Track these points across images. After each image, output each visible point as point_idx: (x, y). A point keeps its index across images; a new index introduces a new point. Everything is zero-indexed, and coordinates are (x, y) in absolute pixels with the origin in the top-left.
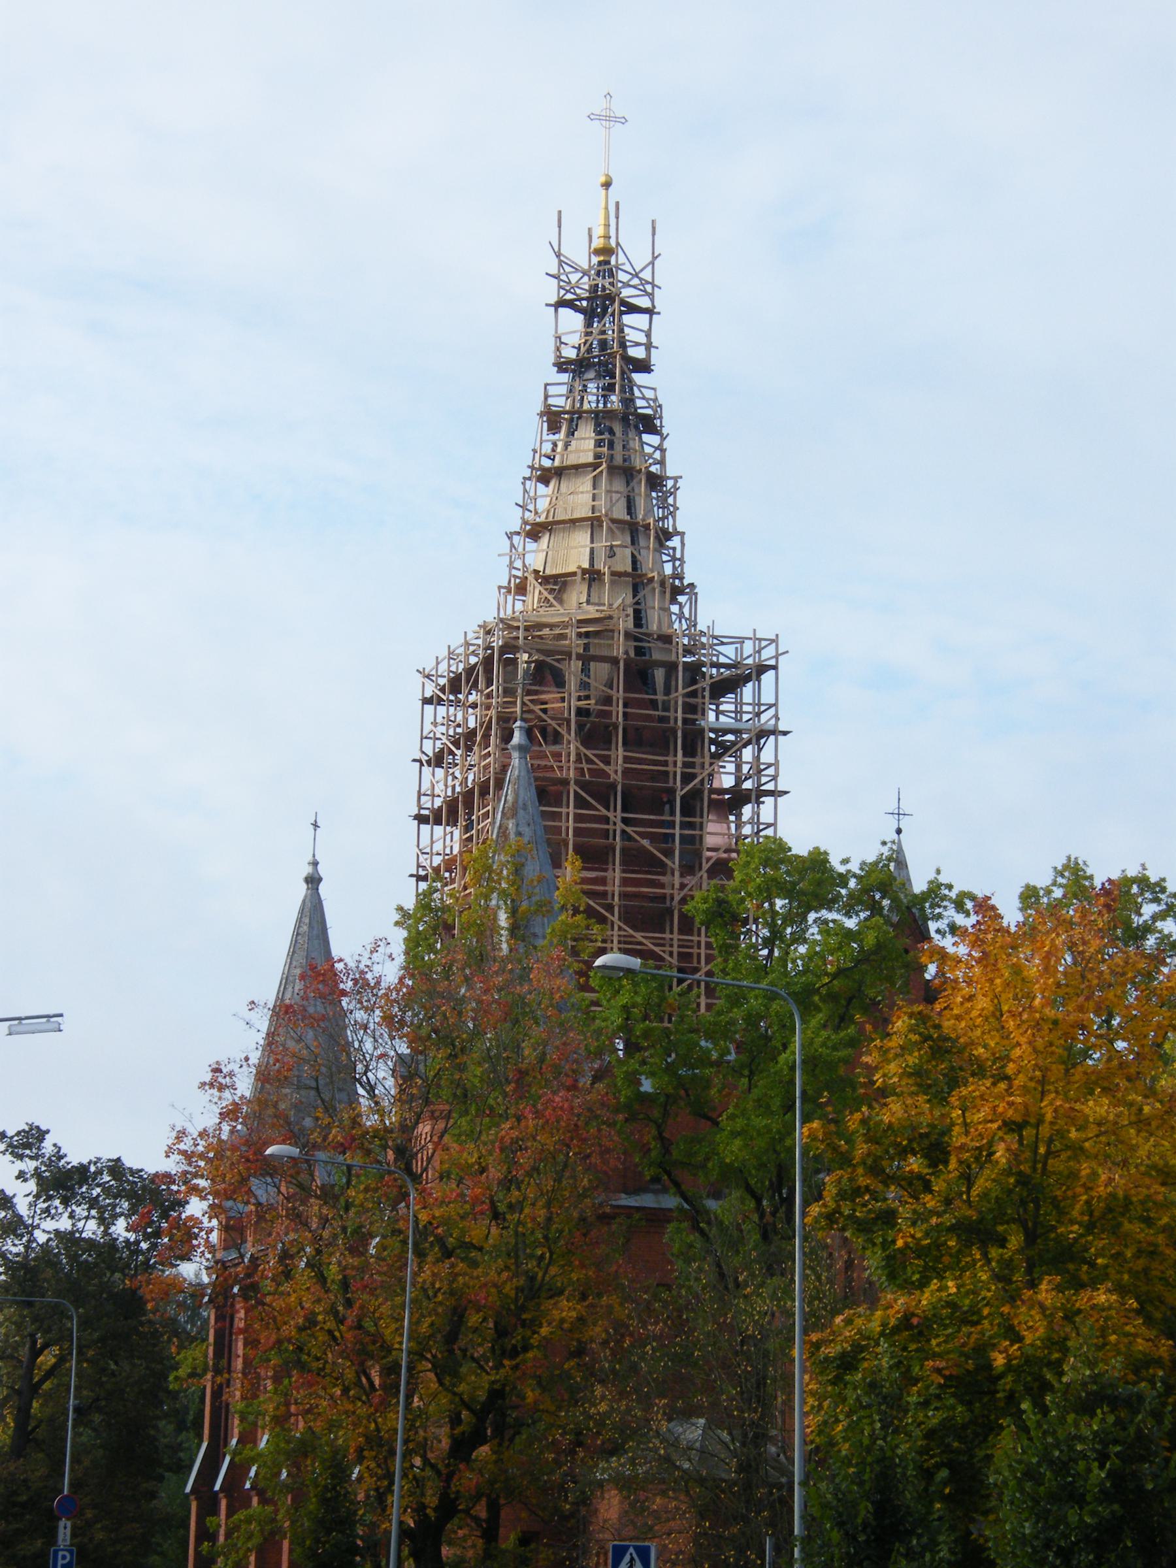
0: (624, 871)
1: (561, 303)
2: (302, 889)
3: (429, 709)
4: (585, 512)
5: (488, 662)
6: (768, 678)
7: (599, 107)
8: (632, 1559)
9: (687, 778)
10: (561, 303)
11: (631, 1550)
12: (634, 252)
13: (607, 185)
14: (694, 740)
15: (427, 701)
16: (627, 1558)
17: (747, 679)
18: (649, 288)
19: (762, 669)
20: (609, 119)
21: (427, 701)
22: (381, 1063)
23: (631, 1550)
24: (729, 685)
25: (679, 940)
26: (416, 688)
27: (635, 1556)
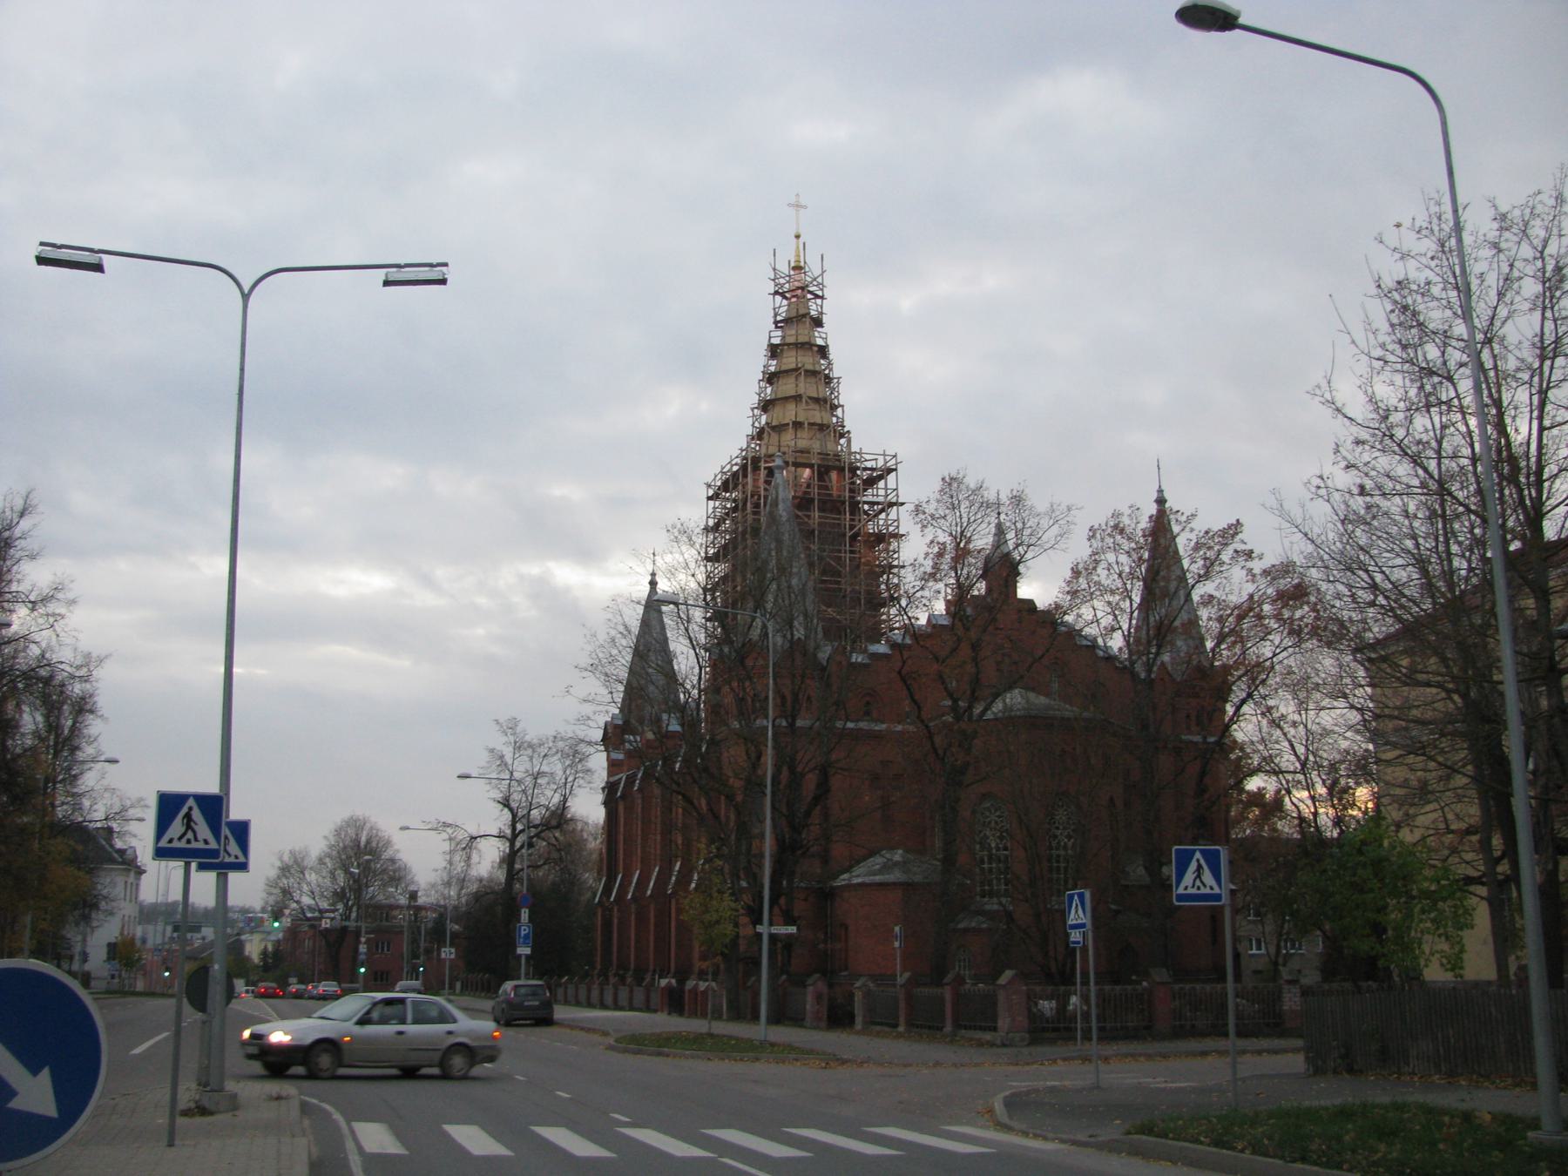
0: (755, 1017)
1: (777, 293)
2: (648, 588)
3: (711, 503)
4: (793, 366)
5: (744, 467)
6: (891, 477)
7: (793, 200)
8: (1200, 867)
9: (852, 527)
10: (777, 293)
11: (1198, 855)
12: (814, 268)
13: (798, 237)
14: (855, 506)
15: (709, 498)
16: (1193, 866)
17: (881, 477)
18: (821, 286)
19: (890, 471)
20: (798, 206)
21: (709, 498)
22: (687, 661)
23: (1198, 855)
24: (871, 482)
25: (771, 924)
26: (704, 492)
27: (1202, 862)
